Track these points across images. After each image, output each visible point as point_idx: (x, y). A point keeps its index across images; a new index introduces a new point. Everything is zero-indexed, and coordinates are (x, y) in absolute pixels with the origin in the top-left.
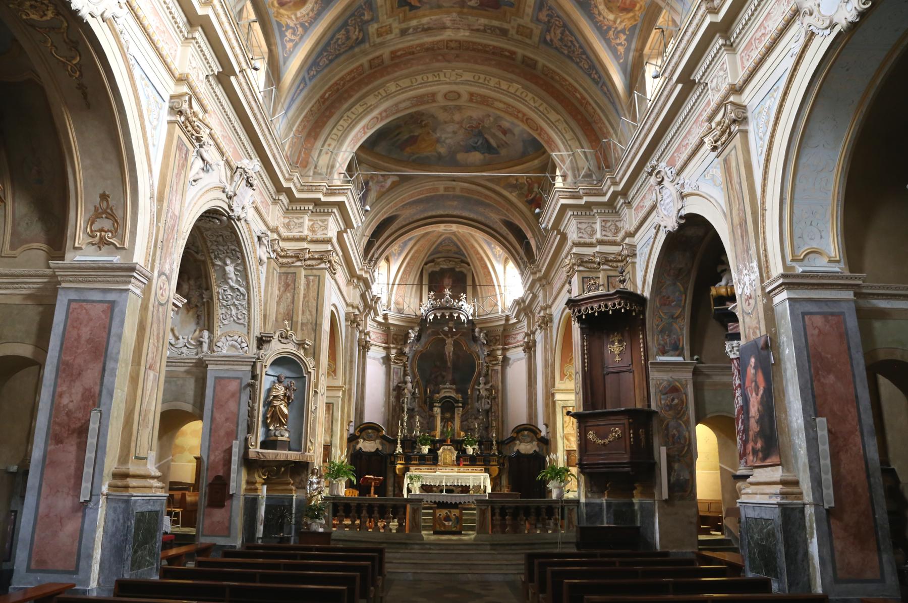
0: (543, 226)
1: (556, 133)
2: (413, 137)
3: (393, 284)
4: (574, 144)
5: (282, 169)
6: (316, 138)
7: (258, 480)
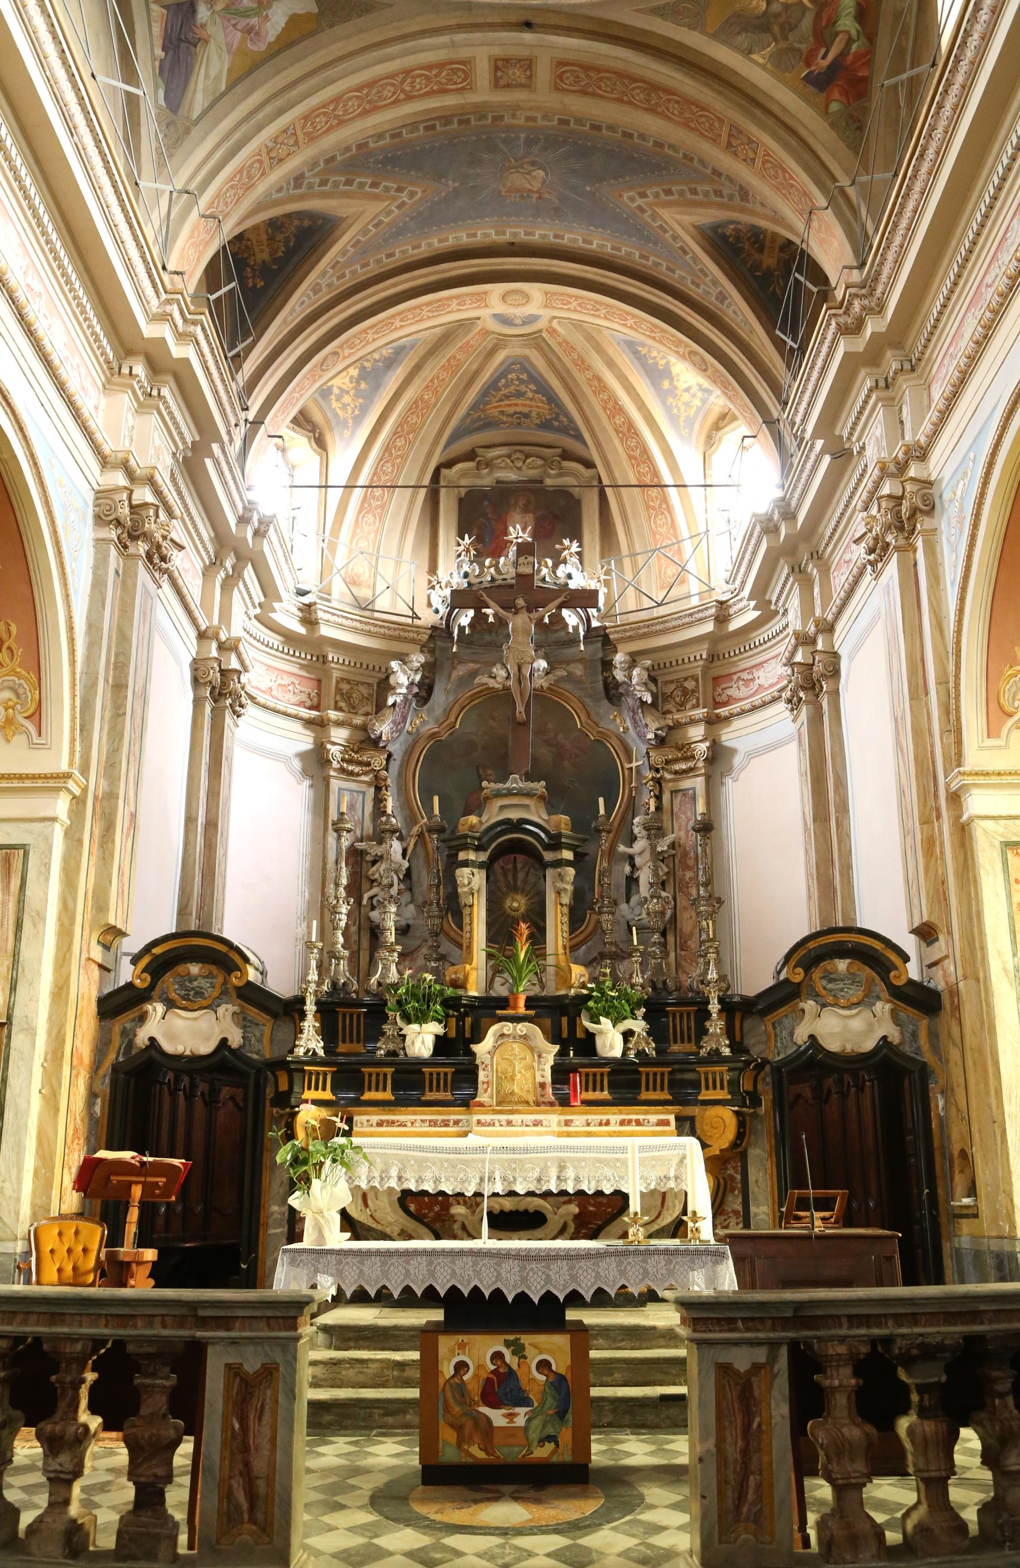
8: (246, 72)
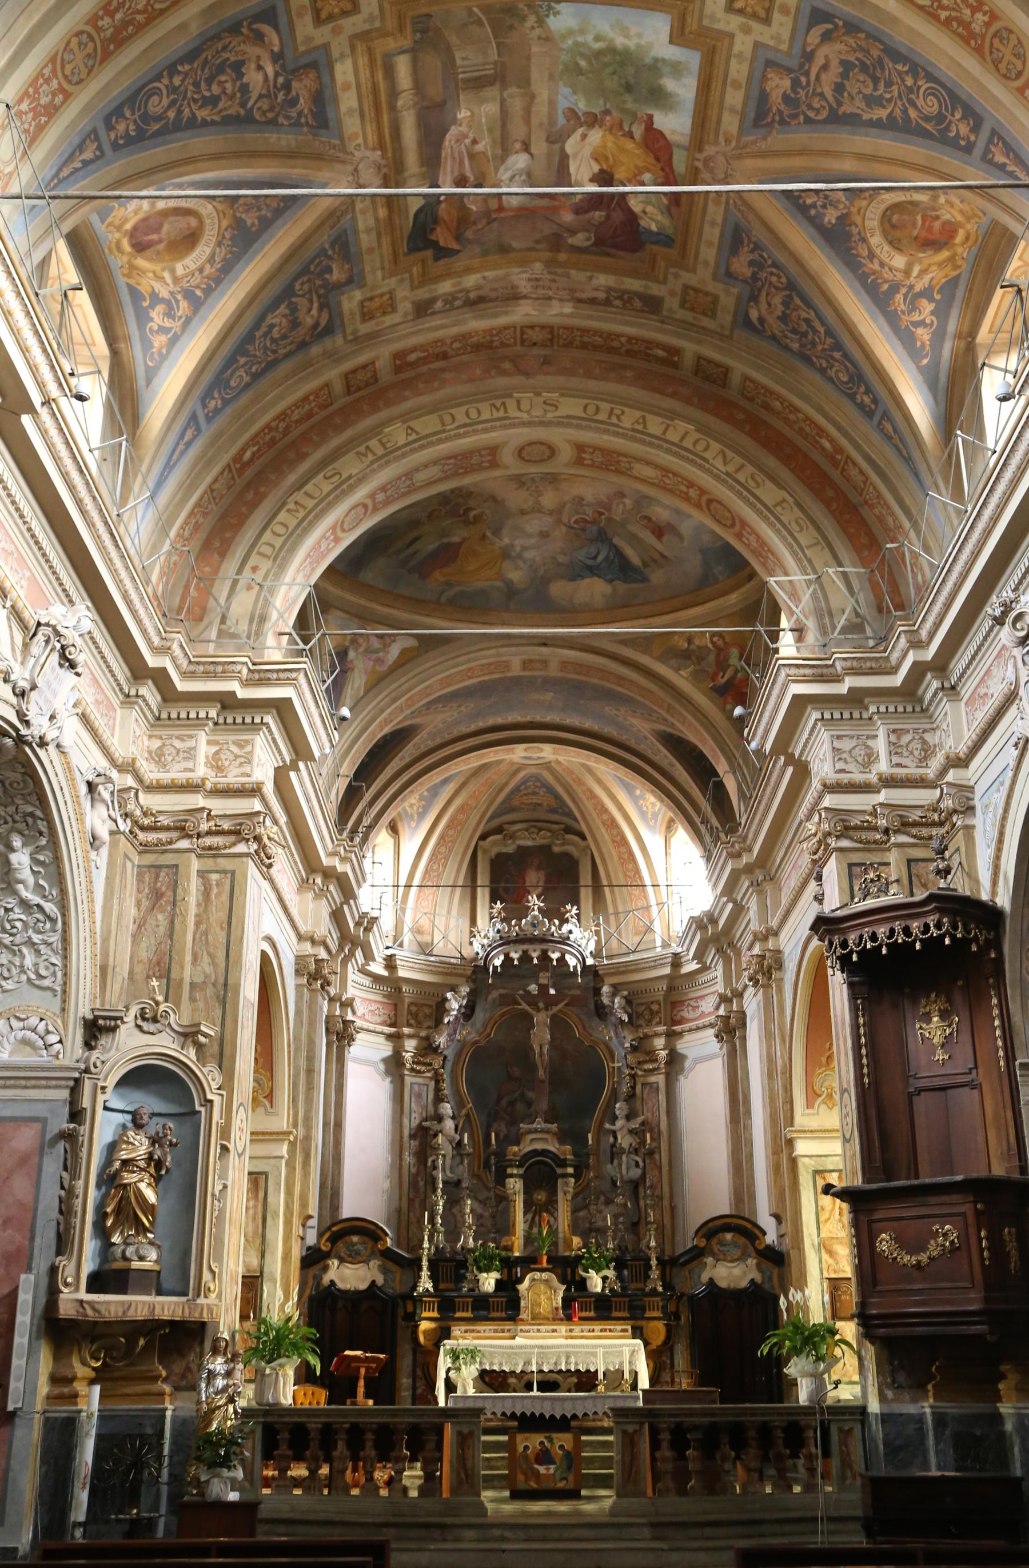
0: (754, 745)
1: (778, 532)
2: (448, 546)
3: (408, 886)
4: (819, 556)
5: (143, 625)
6: (223, 554)
7: (82, 1371)
8: (375, 683)
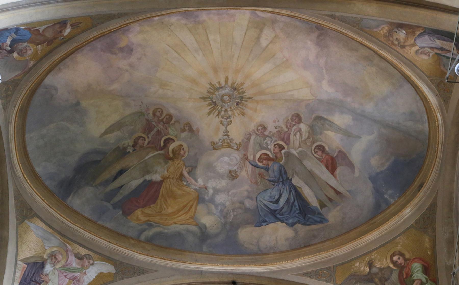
2: (151, 184)
